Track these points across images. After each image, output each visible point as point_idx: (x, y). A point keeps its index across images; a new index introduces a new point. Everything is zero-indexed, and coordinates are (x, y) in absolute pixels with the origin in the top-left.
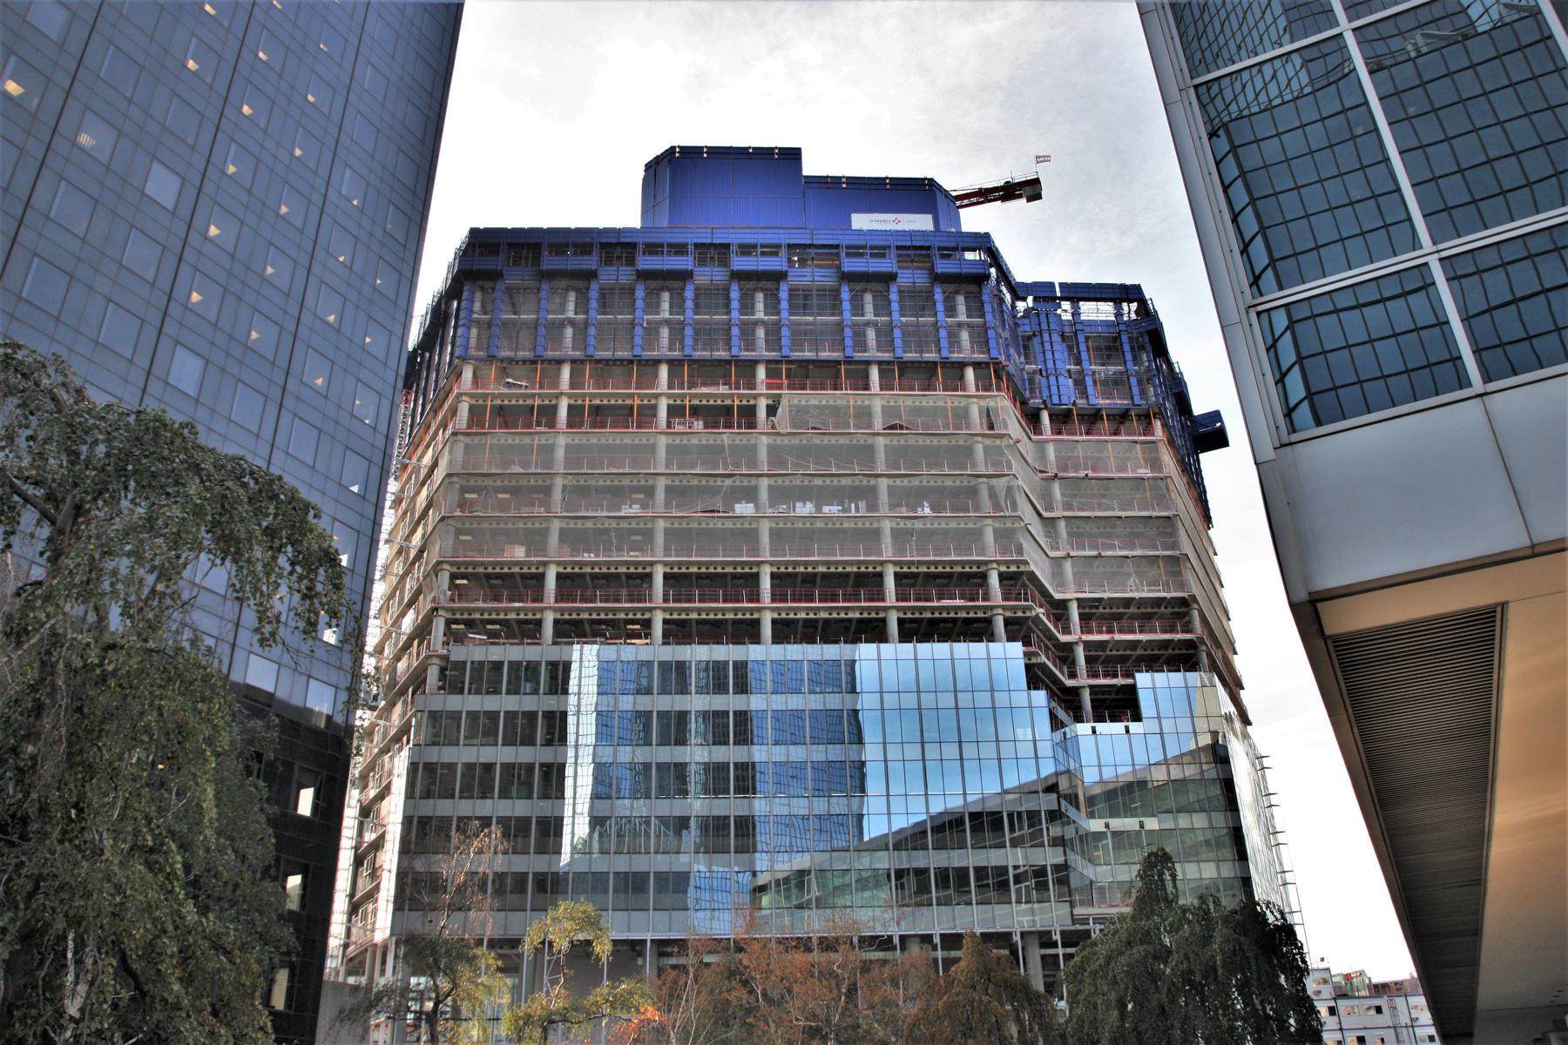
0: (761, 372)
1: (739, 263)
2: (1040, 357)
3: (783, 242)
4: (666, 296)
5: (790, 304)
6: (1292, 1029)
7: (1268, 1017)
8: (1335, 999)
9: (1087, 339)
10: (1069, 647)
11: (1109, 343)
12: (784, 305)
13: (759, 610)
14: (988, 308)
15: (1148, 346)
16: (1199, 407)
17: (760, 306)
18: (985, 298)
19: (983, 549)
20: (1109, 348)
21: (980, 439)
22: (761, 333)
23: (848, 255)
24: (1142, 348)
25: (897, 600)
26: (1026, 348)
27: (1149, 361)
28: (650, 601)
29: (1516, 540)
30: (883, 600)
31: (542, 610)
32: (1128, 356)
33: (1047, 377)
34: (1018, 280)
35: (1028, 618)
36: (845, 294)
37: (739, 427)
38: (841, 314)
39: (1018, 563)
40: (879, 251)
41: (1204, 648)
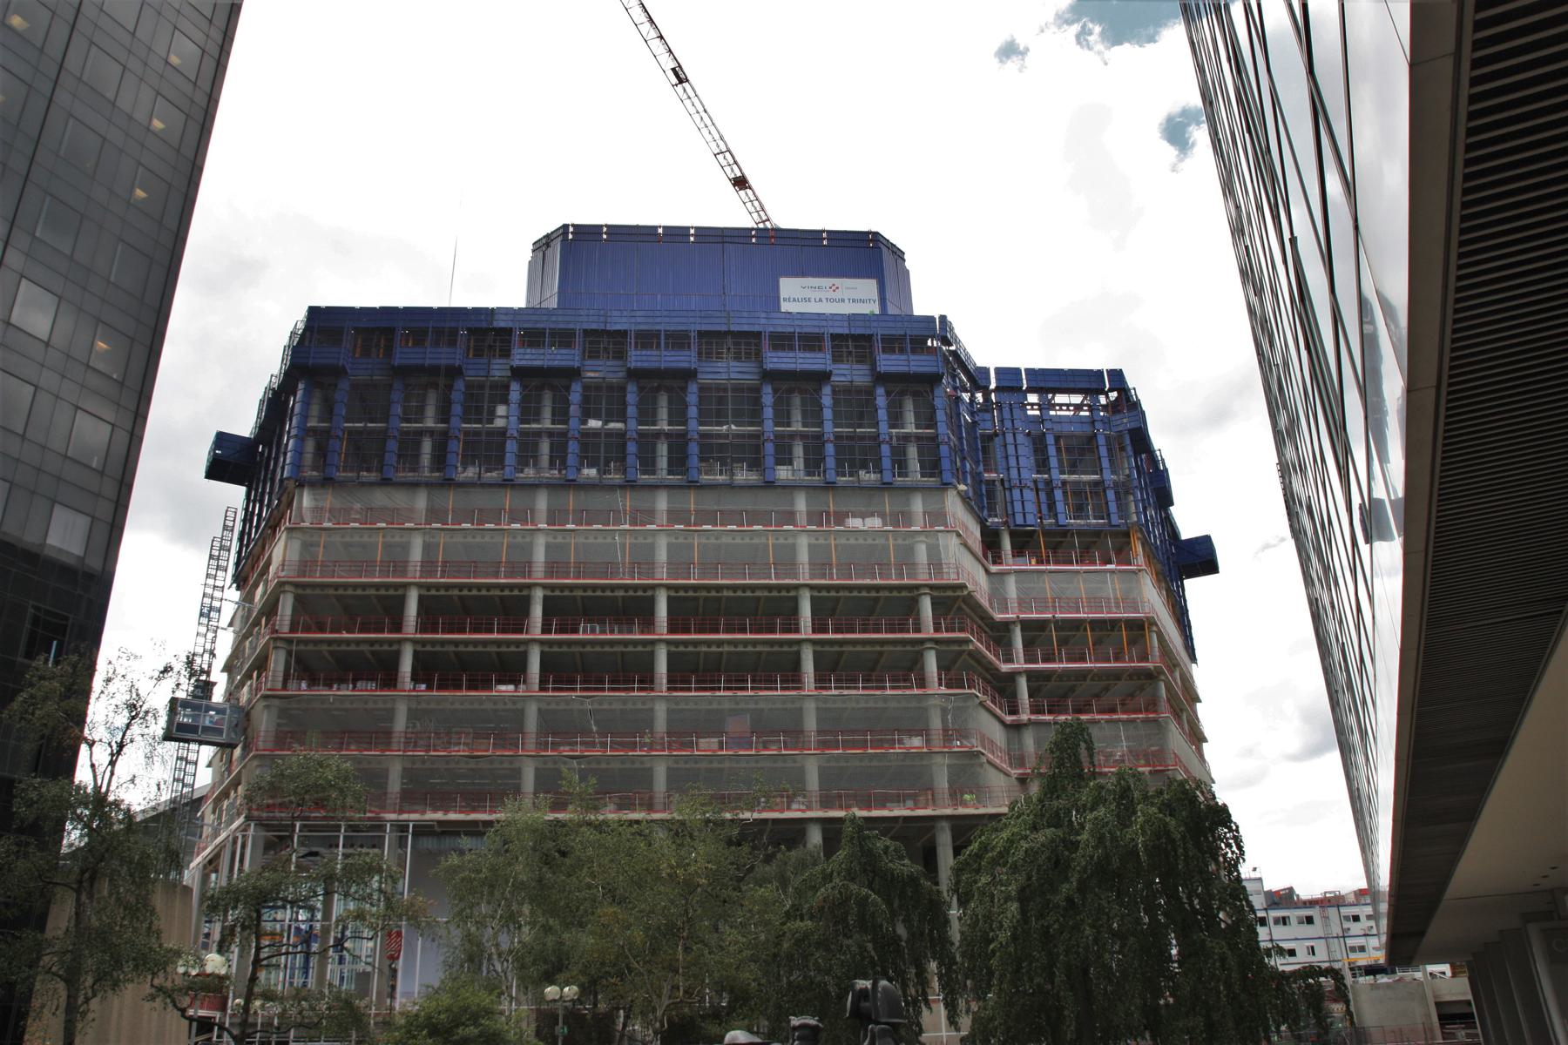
1: (638, 358)
2: (1001, 463)
5: (700, 410)
6: (1223, 926)
7: (1196, 912)
8: (1266, 909)
9: (1057, 439)
10: (1012, 677)
11: (1080, 448)
12: (693, 412)
16: (1187, 531)
17: (663, 413)
18: (938, 402)
21: (923, 538)
22: (663, 449)
25: (814, 632)
26: (985, 450)
27: (1138, 513)
29: (1433, 391)
30: (797, 631)
33: (1010, 489)
36: (768, 398)
38: (760, 424)
40: (811, 342)
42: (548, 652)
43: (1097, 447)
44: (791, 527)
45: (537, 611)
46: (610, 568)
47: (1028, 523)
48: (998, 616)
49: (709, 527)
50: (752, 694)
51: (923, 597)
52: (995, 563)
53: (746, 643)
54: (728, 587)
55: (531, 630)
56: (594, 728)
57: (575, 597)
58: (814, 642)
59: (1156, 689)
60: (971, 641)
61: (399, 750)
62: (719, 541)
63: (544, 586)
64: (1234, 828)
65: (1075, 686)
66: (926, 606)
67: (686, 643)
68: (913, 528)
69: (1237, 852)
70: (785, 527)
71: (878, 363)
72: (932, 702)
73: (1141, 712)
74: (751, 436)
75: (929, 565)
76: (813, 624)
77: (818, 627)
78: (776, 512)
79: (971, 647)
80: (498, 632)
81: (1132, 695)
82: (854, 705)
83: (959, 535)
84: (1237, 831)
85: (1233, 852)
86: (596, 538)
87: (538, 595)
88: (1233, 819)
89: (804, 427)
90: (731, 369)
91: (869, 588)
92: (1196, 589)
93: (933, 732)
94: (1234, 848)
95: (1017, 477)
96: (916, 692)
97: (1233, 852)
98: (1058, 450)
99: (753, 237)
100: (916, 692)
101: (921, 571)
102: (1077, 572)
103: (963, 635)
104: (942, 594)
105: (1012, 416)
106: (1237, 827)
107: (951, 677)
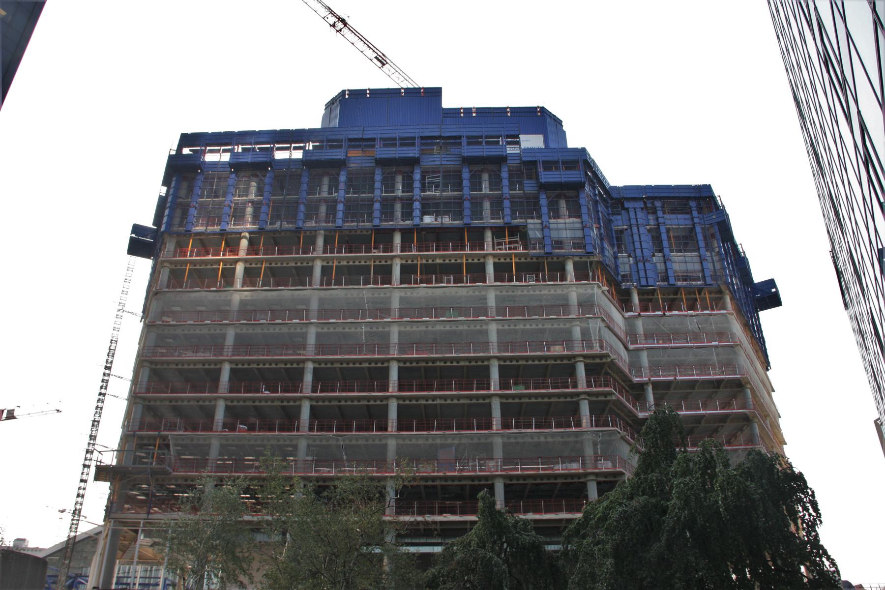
0: (397, 239)
3: (417, 135)
4: (326, 181)
6: (805, 580)
9: (668, 231)
13: (386, 437)
14: (584, 210)
15: (718, 235)
16: (758, 277)
18: (582, 201)
19: (576, 382)
20: (685, 237)
21: (578, 323)
23: (469, 144)
24: (713, 236)
27: (719, 247)
28: (298, 430)
31: (216, 399)
32: (702, 244)
34: (612, 184)
35: (604, 363)
37: (375, 283)
39: (601, 357)
41: (749, 386)
42: (315, 406)
43: (696, 235)
44: (484, 318)
45: (308, 378)
46: (357, 348)
47: (650, 284)
48: (636, 380)
49: (427, 319)
50: (456, 432)
51: (579, 363)
52: (627, 311)
53: (452, 397)
54: (440, 359)
55: (304, 390)
56: (345, 457)
57: (335, 368)
58: (501, 396)
59: (752, 429)
60: (614, 394)
61: (228, 356)
62: (435, 402)
63: (314, 361)
64: (810, 493)
65: (694, 428)
66: (581, 370)
67: (410, 398)
68: (571, 316)
69: (814, 514)
70: (481, 318)
71: (540, 177)
72: (585, 437)
73: (742, 445)
74: (455, 198)
75: (582, 341)
76: (500, 384)
77: (504, 385)
78: (474, 308)
79: (614, 398)
80: (281, 392)
81: (735, 436)
82: (530, 440)
83: (603, 320)
84: (813, 495)
85: (810, 515)
86: (350, 329)
87: (310, 366)
88: (809, 485)
89: (490, 191)
90: (443, 159)
91: (540, 358)
92: (766, 317)
93: (587, 458)
94: (811, 511)
95: (641, 254)
96: (573, 429)
97: (810, 515)
98: (669, 238)
99: (462, 113)
100: (573, 429)
101: (577, 345)
102: (691, 347)
103: (607, 389)
104: (592, 361)
105: (643, 254)
106: (813, 492)
107: (582, 273)
